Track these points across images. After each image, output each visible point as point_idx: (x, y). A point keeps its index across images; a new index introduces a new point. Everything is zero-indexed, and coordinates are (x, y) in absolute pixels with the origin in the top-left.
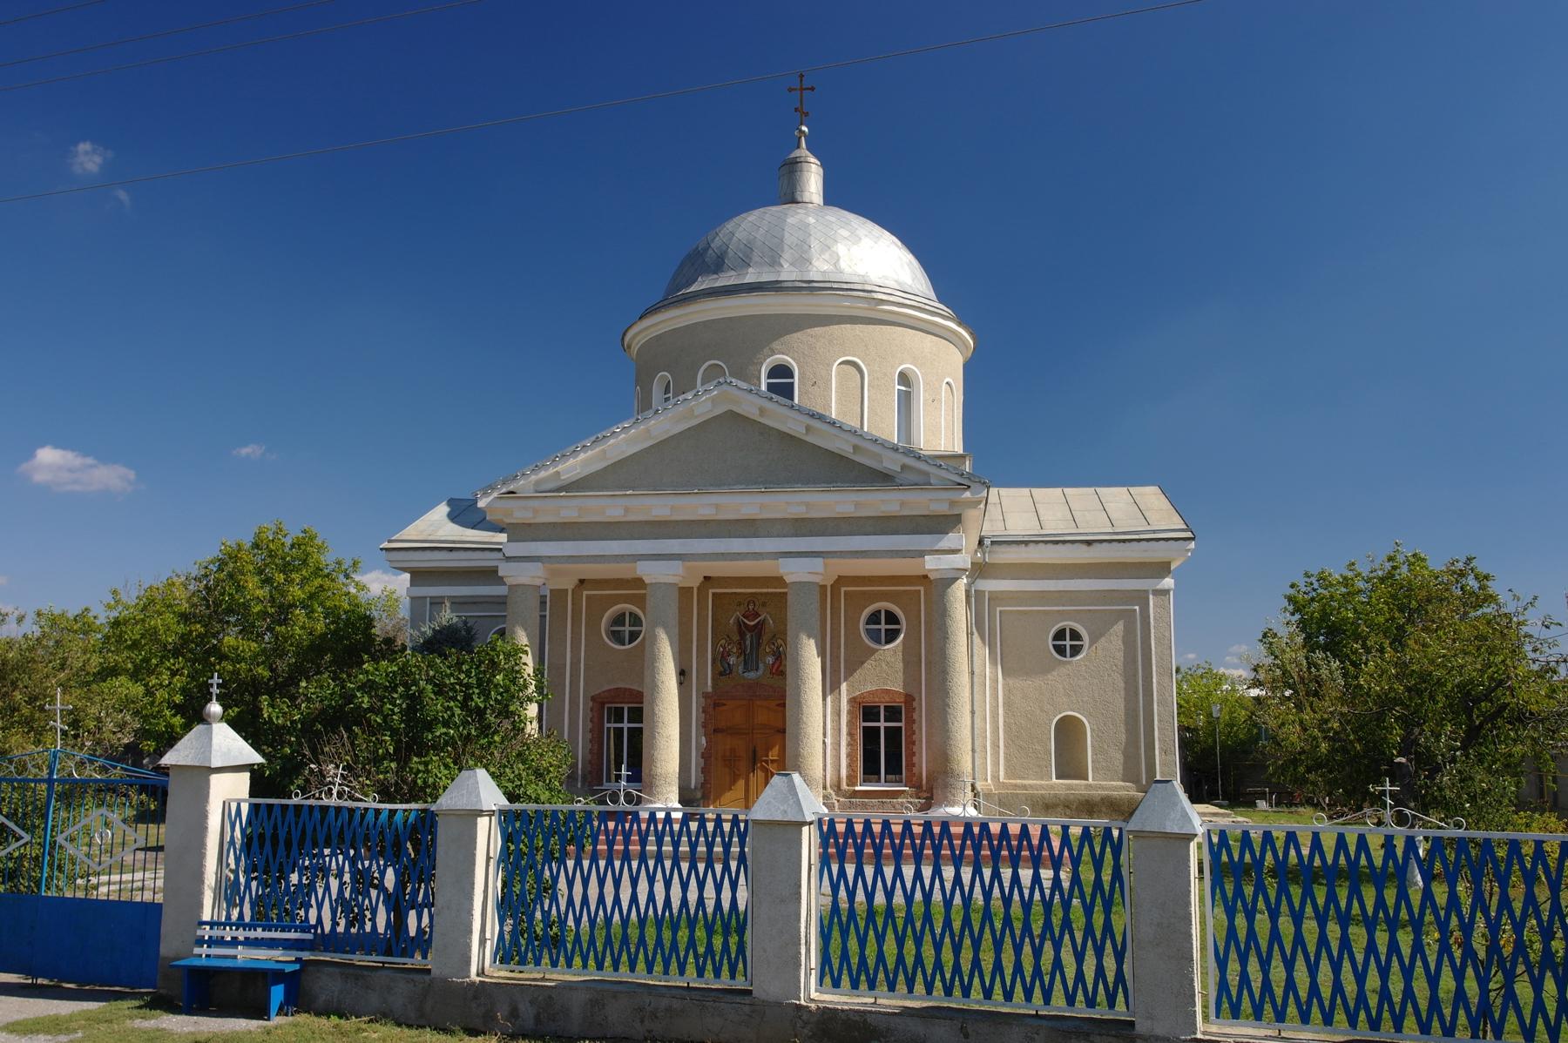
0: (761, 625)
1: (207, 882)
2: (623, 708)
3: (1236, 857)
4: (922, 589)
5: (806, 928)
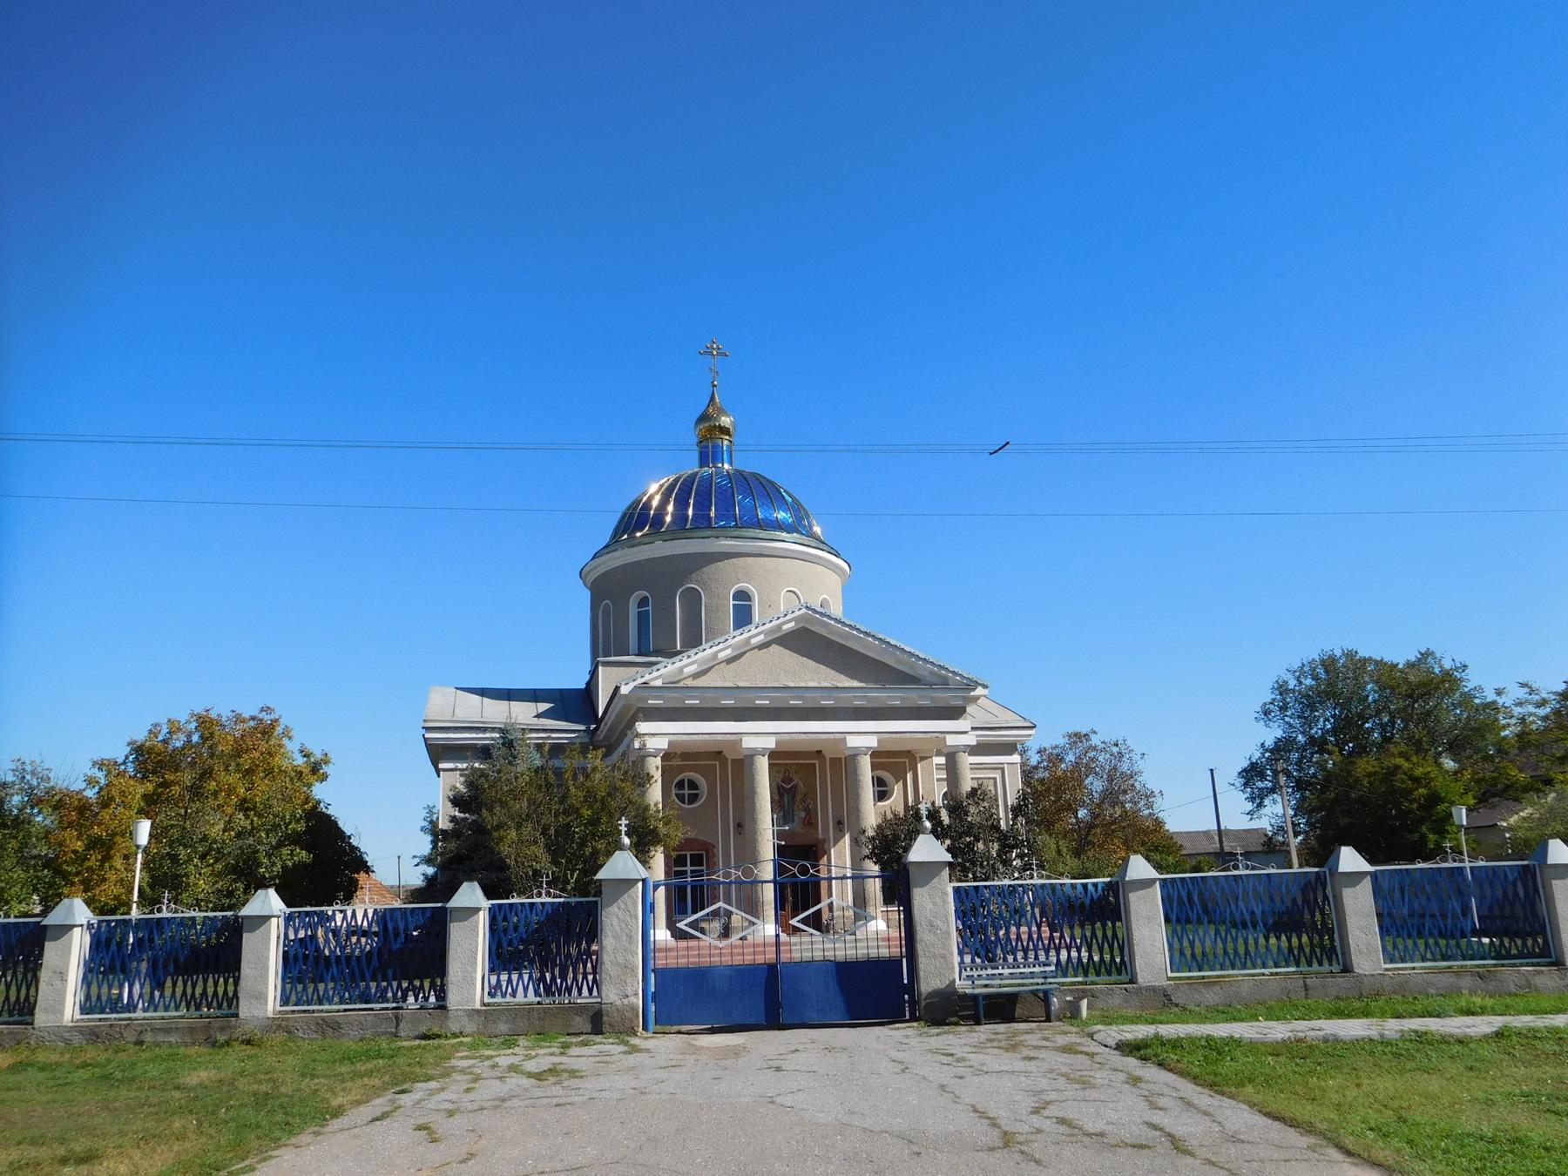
0: (795, 787)
1: (681, 1027)
2: (686, 855)
3: (359, 923)
4: (817, 762)
5: (1277, 973)
